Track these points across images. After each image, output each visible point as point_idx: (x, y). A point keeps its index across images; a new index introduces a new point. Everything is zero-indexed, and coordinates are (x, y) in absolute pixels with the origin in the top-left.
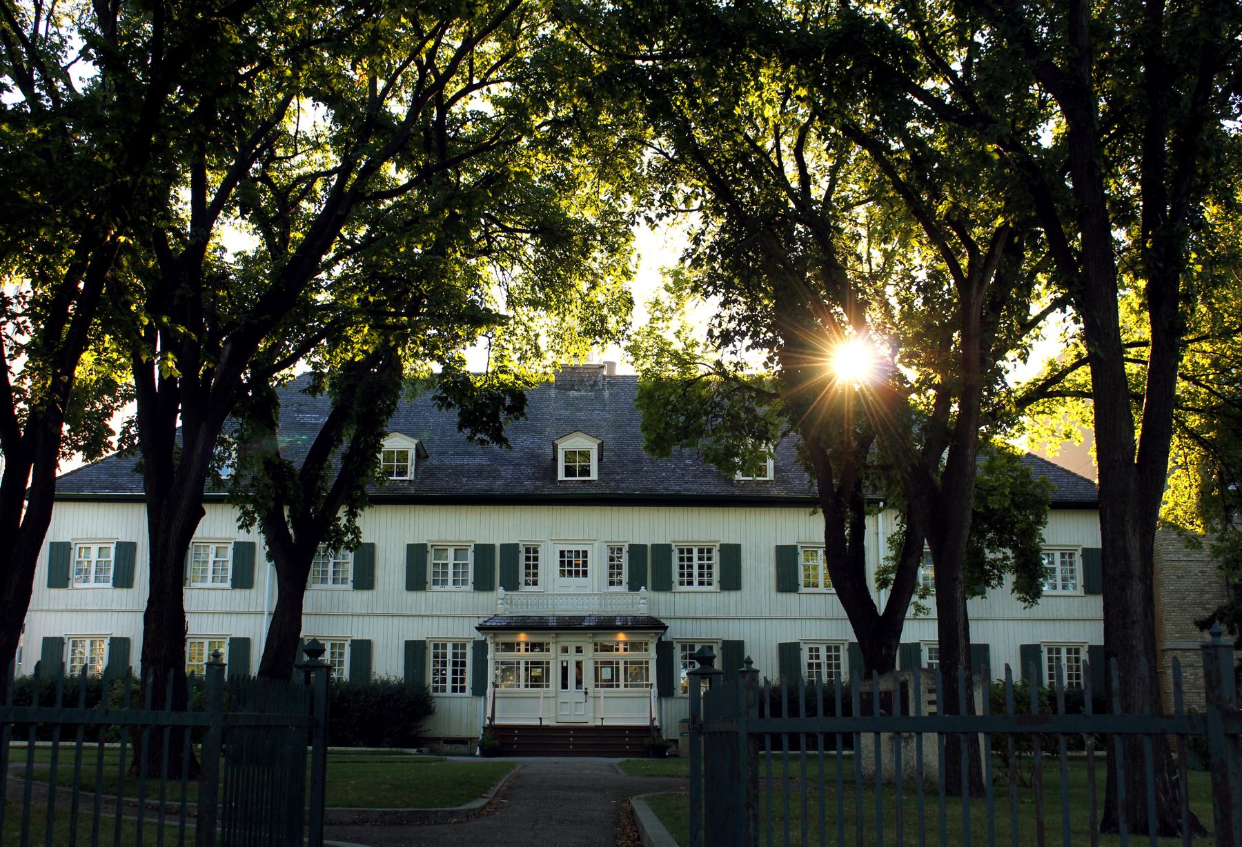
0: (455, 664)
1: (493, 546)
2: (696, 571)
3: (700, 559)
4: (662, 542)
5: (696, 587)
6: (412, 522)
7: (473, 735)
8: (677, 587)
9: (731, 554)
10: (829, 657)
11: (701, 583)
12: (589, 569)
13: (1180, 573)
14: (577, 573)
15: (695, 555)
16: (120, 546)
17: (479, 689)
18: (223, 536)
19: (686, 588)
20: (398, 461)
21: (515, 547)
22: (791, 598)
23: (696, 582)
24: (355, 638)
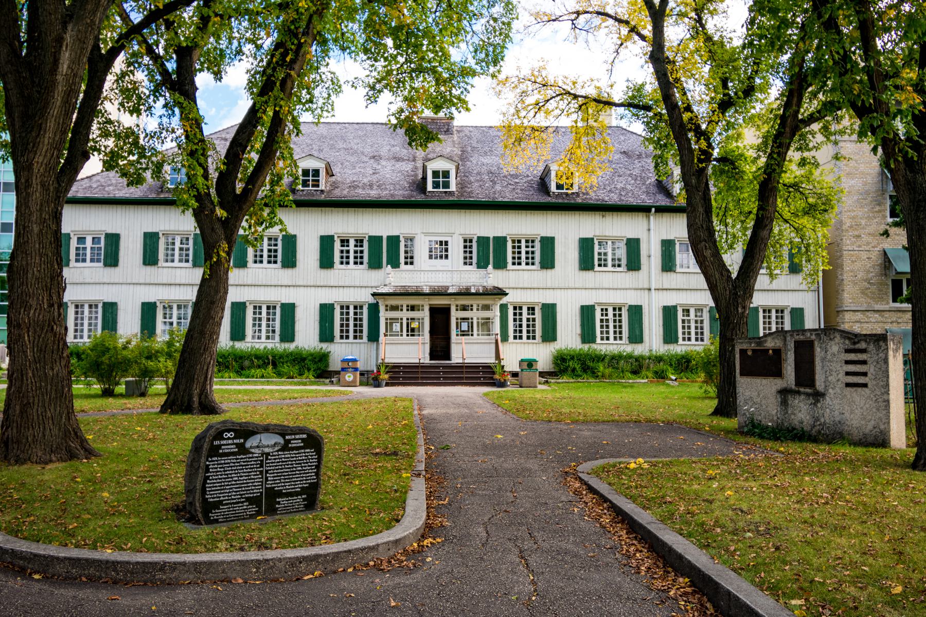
0: (355, 319)
1: (488, 238)
2: (523, 255)
3: (527, 247)
4: (500, 235)
5: (523, 266)
6: (127, 219)
7: (369, 369)
8: (161, 263)
9: (548, 244)
10: (615, 315)
11: (527, 264)
12: (449, 253)
13: (854, 258)
14: (441, 257)
15: (523, 244)
16: (108, 236)
17: (374, 337)
18: (186, 229)
19: (170, 264)
20: (313, 176)
21: (504, 239)
22: (589, 274)
23: (523, 264)
24: (283, 302)
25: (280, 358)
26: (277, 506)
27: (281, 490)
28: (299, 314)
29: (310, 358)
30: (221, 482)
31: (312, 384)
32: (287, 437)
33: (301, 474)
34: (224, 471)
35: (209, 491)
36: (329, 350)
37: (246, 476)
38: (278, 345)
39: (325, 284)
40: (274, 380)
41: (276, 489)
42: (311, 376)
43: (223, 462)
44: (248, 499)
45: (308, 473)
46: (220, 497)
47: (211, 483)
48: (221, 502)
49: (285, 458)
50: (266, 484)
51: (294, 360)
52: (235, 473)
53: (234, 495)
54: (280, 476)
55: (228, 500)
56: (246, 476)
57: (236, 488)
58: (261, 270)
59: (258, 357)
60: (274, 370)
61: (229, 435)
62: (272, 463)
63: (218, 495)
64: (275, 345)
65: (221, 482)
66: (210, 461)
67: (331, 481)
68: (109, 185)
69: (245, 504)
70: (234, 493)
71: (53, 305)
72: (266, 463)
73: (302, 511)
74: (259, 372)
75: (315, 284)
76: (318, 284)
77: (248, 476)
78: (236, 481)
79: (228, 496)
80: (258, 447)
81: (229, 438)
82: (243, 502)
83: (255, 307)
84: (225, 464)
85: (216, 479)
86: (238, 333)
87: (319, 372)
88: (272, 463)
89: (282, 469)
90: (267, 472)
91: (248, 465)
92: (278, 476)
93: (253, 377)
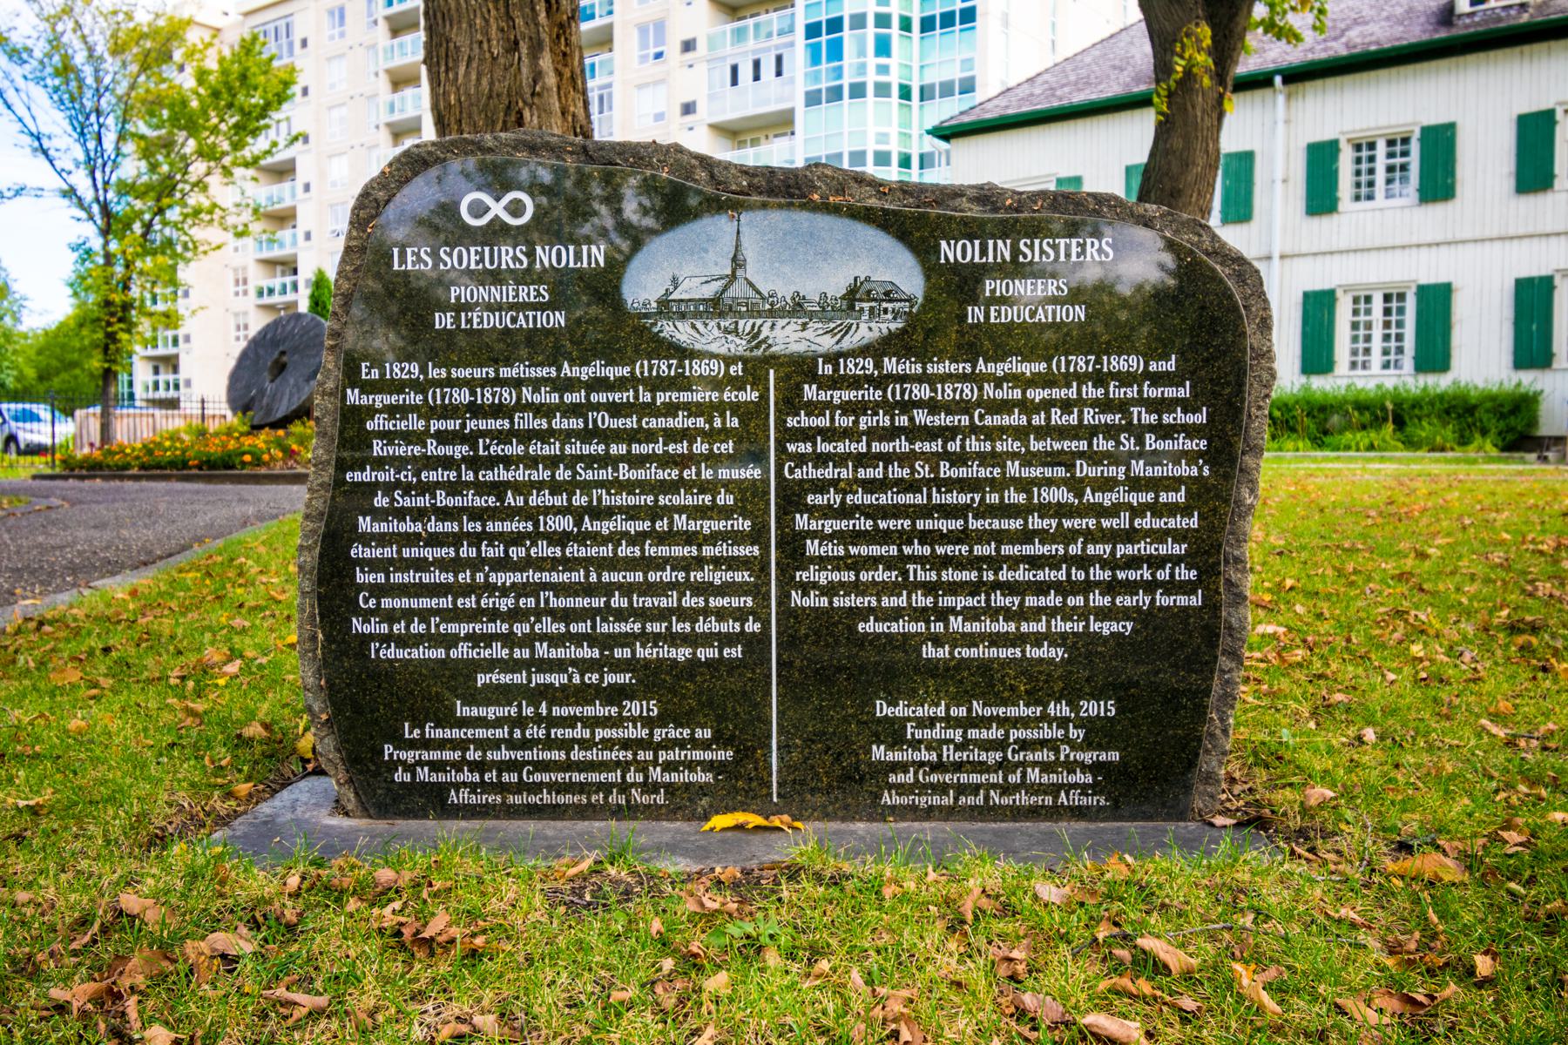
24: (1424, 281)
25: (1413, 407)
26: (879, 752)
27: (907, 642)
28: (1461, 308)
29: (1489, 405)
30: (455, 540)
31: (1490, 460)
32: (949, 251)
33: (1068, 537)
34: (474, 463)
35: (378, 591)
36: (1538, 387)
37: (632, 513)
38: (1410, 381)
39: (1531, 230)
40: (1398, 454)
41: (869, 627)
42: (1489, 446)
43: (462, 396)
44: (651, 678)
45: (1130, 536)
46: (450, 641)
47: (383, 540)
48: (459, 677)
49: (933, 407)
50: (787, 583)
51: (1447, 412)
52: (555, 488)
53: (555, 641)
54: (905, 538)
55: (511, 666)
56: (632, 513)
57: (560, 589)
58: (1369, 215)
59: (1361, 406)
60: (1398, 434)
61: (497, 209)
62: (830, 434)
63: (437, 625)
64: (1405, 380)
65: (455, 540)
66: (368, 388)
67: (1417, 649)
68: (1063, 86)
69: (634, 708)
70: (549, 626)
71: (514, 46)
72: (787, 435)
73: (1079, 813)
74: (1362, 438)
75: (1503, 234)
76: (1512, 232)
77: (654, 513)
78: (561, 539)
79: (509, 640)
80: (715, 307)
81: (496, 233)
82: (615, 695)
83: (1356, 300)
84: (475, 410)
85: (419, 514)
86: (1317, 358)
87: (1510, 437)
88: (830, 434)
89: (911, 486)
90: (792, 497)
91: (650, 436)
92: (885, 537)
93: (1347, 448)
